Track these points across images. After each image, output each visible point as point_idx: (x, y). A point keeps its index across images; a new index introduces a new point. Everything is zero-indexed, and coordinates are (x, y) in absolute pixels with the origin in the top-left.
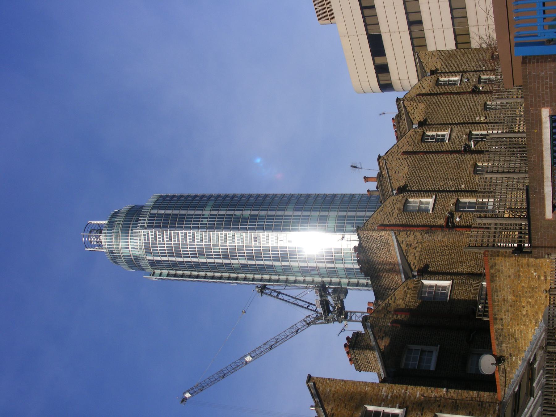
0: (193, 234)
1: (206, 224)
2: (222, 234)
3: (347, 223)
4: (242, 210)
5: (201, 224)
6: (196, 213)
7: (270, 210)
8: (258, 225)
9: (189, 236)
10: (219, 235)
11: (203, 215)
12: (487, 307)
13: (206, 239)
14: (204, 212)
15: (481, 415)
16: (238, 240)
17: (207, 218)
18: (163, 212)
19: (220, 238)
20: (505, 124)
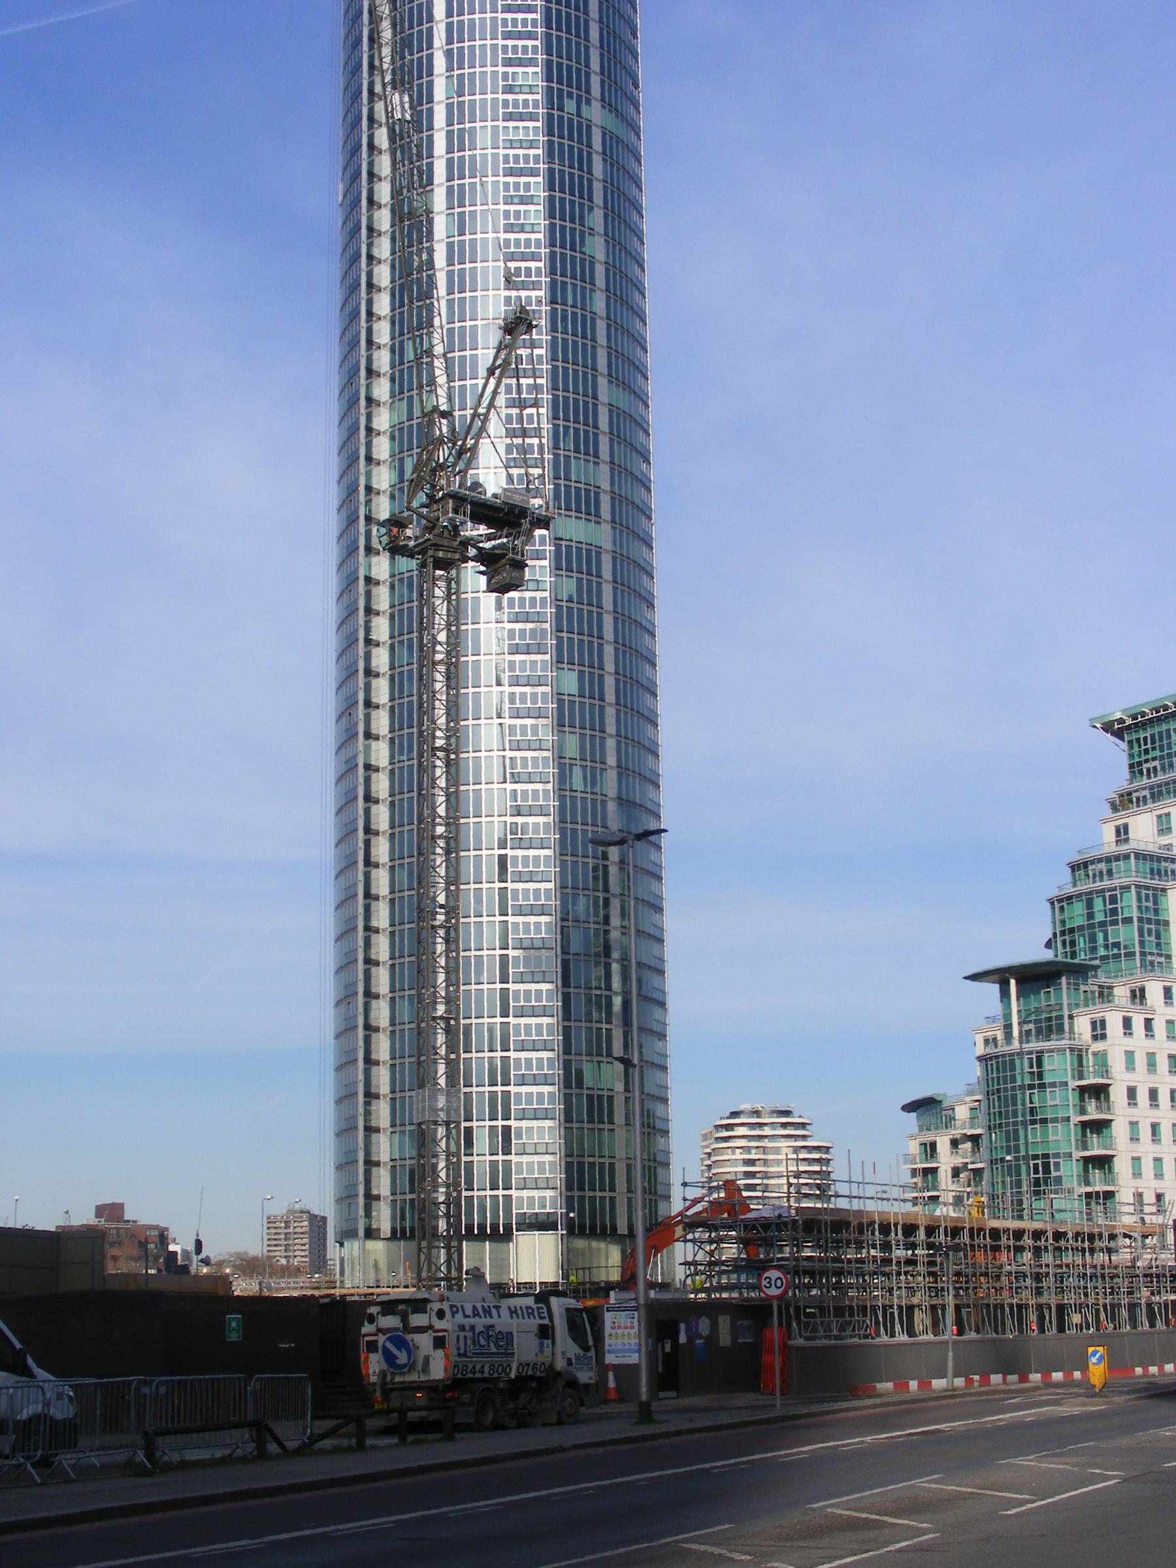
0: (532, 63)
1: (561, 109)
2: (536, 161)
3: (579, 580)
4: (606, 234)
5: (560, 91)
6: (591, 23)
7: (602, 82)
8: (564, 284)
9: (525, 21)
10: (532, 152)
11: (588, 102)
12: (1145, 803)
13: (516, 106)
14: (596, 105)
15: (100, 1210)
16: (517, 213)
17: (579, 115)
18: (595, 65)
19: (521, 152)
20: (1150, 904)
